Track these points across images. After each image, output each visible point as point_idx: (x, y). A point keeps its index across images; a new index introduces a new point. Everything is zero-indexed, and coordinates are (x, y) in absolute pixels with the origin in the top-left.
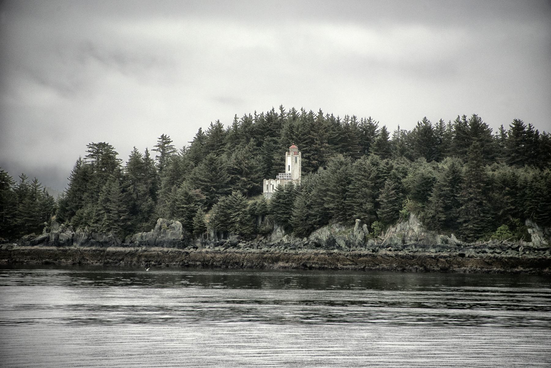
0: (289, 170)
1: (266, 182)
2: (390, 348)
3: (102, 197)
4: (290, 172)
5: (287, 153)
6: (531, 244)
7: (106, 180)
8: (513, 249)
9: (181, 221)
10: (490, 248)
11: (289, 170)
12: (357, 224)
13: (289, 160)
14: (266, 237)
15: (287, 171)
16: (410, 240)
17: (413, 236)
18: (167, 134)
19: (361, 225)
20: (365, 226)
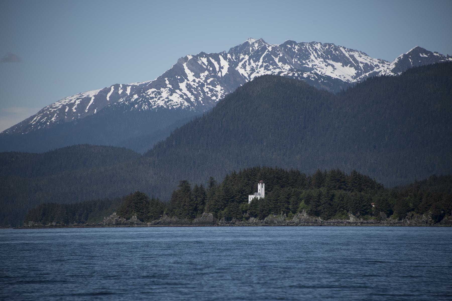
3: (182, 204)
6: (349, 221)
13: (259, 186)
15: (259, 192)
19: (283, 214)
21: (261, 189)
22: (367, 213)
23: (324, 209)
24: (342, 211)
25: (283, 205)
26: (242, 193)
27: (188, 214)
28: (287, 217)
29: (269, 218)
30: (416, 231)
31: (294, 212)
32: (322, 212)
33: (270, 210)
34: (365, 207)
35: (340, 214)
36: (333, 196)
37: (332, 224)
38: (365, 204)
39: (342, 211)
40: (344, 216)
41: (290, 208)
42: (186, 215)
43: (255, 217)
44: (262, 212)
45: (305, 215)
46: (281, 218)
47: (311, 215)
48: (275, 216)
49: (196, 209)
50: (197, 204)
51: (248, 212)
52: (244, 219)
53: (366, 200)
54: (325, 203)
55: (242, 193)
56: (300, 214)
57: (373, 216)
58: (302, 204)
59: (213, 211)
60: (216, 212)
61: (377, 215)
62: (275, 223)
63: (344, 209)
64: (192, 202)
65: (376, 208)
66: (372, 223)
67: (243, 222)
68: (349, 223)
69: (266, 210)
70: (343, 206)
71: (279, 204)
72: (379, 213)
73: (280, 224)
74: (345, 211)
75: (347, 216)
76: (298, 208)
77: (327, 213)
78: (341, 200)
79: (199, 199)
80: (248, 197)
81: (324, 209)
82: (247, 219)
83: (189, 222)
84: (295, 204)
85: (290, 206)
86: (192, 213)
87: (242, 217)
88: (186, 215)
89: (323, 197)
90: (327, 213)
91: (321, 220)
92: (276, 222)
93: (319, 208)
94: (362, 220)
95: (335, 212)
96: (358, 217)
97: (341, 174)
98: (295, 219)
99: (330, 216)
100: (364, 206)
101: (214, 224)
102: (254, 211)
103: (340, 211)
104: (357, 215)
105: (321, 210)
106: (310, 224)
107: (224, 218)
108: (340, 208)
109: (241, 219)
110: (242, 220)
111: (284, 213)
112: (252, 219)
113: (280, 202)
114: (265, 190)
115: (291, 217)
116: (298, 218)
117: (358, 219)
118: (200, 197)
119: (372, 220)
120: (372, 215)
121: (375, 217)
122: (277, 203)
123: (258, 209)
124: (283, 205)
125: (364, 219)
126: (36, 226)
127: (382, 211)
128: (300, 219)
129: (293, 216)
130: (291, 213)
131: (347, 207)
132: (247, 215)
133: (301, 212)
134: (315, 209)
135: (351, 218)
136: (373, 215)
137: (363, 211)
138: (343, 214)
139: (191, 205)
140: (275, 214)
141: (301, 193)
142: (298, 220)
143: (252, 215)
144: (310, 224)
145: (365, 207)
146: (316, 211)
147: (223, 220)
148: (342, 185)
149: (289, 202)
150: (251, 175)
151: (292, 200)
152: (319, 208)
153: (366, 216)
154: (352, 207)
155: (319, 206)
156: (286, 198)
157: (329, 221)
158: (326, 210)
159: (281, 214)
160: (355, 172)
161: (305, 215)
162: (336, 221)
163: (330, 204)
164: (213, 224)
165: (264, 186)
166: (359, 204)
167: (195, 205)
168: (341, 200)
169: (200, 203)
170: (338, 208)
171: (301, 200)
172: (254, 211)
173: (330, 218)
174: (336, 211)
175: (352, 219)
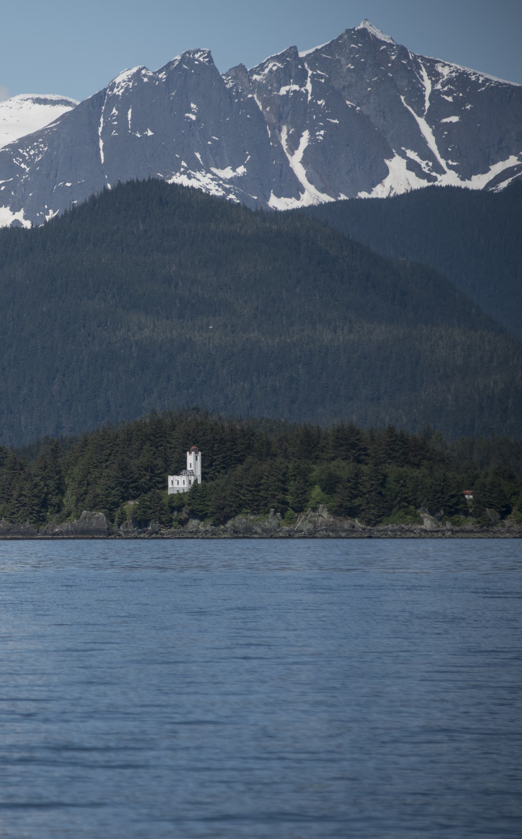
0: (191, 467)
1: (170, 478)
2: (191, 557)
3: (15, 493)
4: (192, 469)
5: (188, 453)
6: (423, 527)
7: (139, 455)
8: (410, 532)
9: (104, 513)
10: (391, 531)
11: (191, 467)
12: (272, 513)
13: (190, 458)
14: (183, 526)
15: (189, 468)
16: (321, 525)
17: (323, 522)
18: (446, 174)
19: (275, 514)
20: (279, 514)
21: (193, 461)
22: (457, 512)
23: (368, 503)
24: (405, 507)
25: (274, 496)
26: (152, 471)
27: (31, 513)
28: (283, 518)
29: (240, 520)
30: (35, 731)
31: (300, 510)
32: (363, 510)
33: (240, 506)
34: (454, 500)
35: (401, 513)
36: (385, 476)
37: (389, 533)
38: (454, 493)
39: (405, 507)
40: (409, 517)
41: (290, 501)
42: (27, 515)
43: (202, 518)
44: (223, 509)
45: (325, 514)
46: (271, 521)
47: (339, 515)
48: (252, 518)
49: (45, 504)
50: (47, 494)
51: (186, 510)
52: (175, 523)
53: (455, 485)
54: (369, 492)
55: (152, 471)
56: (312, 514)
57: (470, 518)
58: (316, 492)
59: (104, 508)
60: (110, 510)
61: (478, 514)
62: (256, 533)
63: (408, 502)
64: (36, 491)
65: (476, 501)
66: (472, 531)
67: (173, 529)
68: (425, 531)
69: (231, 506)
70: (406, 498)
71: (262, 493)
72: (485, 511)
73: (270, 534)
74: (412, 507)
75: (417, 516)
76: (307, 501)
77: (372, 511)
78: (403, 486)
79: (52, 484)
80: (165, 481)
81: (368, 503)
82: (183, 523)
83: (35, 530)
84: (301, 494)
85: (289, 498)
86: (39, 512)
87: (171, 520)
88: (27, 515)
89: (364, 478)
90: (372, 511)
91: (359, 524)
92: (259, 530)
93: (357, 502)
94: (448, 525)
95: (391, 510)
96: (440, 519)
97: (358, 433)
98: (302, 523)
99: (379, 516)
100: (453, 496)
101: (110, 534)
102: (200, 507)
103: (400, 508)
104: (438, 514)
105: (360, 505)
106: (343, 534)
107: (129, 521)
108: (399, 502)
109: (168, 524)
110: (171, 526)
111: (276, 512)
112: (193, 523)
113: (267, 490)
114: (203, 467)
115: (292, 520)
116: (310, 522)
117: (440, 523)
118: (51, 478)
119: (469, 524)
120: (466, 514)
121: (475, 519)
122: (259, 491)
123: (210, 503)
124: (274, 496)
125: (454, 523)
126: (57, 534)
127: (489, 508)
128: (314, 523)
129: (297, 518)
130: (290, 511)
131: (415, 499)
132: (184, 515)
133: (314, 509)
134: (348, 504)
135: (425, 520)
136: (471, 514)
137: (451, 507)
138: (407, 513)
139: (35, 496)
140: (255, 514)
141: (311, 470)
142: (310, 526)
143: (193, 514)
144: (343, 534)
145: (454, 500)
146: (350, 508)
147: (129, 525)
148: (360, 455)
149: (286, 490)
150: (154, 436)
151: (292, 486)
152: (357, 502)
153: (455, 518)
154: (428, 500)
155: (356, 497)
156: (279, 480)
157: (380, 527)
158: (372, 505)
159: (268, 512)
160: (391, 430)
161: (324, 516)
162: (396, 527)
163: (380, 493)
164: (108, 534)
165: (199, 458)
166: (442, 493)
167: (43, 496)
168: (403, 486)
169: (54, 491)
170: (396, 502)
171: (312, 485)
172: (200, 507)
173: (380, 522)
174: (393, 508)
175: (428, 523)
